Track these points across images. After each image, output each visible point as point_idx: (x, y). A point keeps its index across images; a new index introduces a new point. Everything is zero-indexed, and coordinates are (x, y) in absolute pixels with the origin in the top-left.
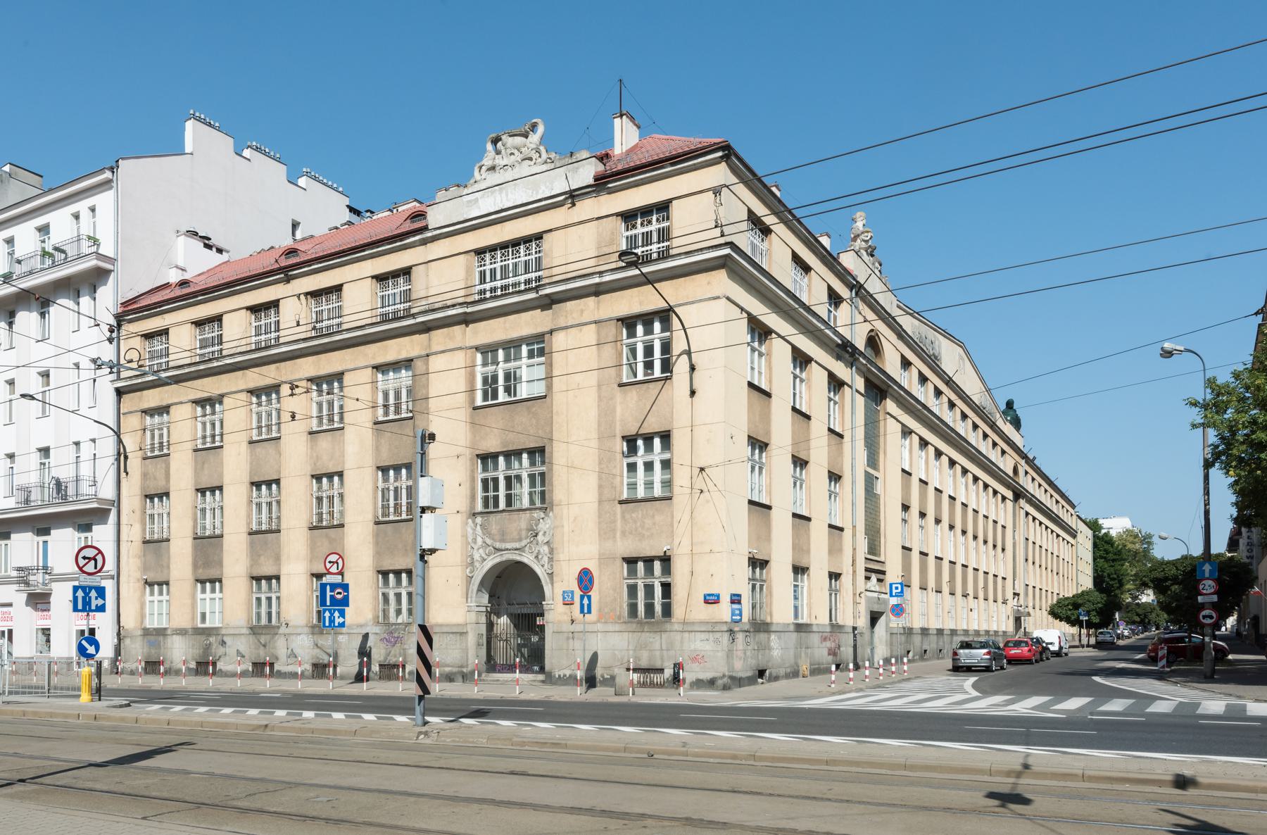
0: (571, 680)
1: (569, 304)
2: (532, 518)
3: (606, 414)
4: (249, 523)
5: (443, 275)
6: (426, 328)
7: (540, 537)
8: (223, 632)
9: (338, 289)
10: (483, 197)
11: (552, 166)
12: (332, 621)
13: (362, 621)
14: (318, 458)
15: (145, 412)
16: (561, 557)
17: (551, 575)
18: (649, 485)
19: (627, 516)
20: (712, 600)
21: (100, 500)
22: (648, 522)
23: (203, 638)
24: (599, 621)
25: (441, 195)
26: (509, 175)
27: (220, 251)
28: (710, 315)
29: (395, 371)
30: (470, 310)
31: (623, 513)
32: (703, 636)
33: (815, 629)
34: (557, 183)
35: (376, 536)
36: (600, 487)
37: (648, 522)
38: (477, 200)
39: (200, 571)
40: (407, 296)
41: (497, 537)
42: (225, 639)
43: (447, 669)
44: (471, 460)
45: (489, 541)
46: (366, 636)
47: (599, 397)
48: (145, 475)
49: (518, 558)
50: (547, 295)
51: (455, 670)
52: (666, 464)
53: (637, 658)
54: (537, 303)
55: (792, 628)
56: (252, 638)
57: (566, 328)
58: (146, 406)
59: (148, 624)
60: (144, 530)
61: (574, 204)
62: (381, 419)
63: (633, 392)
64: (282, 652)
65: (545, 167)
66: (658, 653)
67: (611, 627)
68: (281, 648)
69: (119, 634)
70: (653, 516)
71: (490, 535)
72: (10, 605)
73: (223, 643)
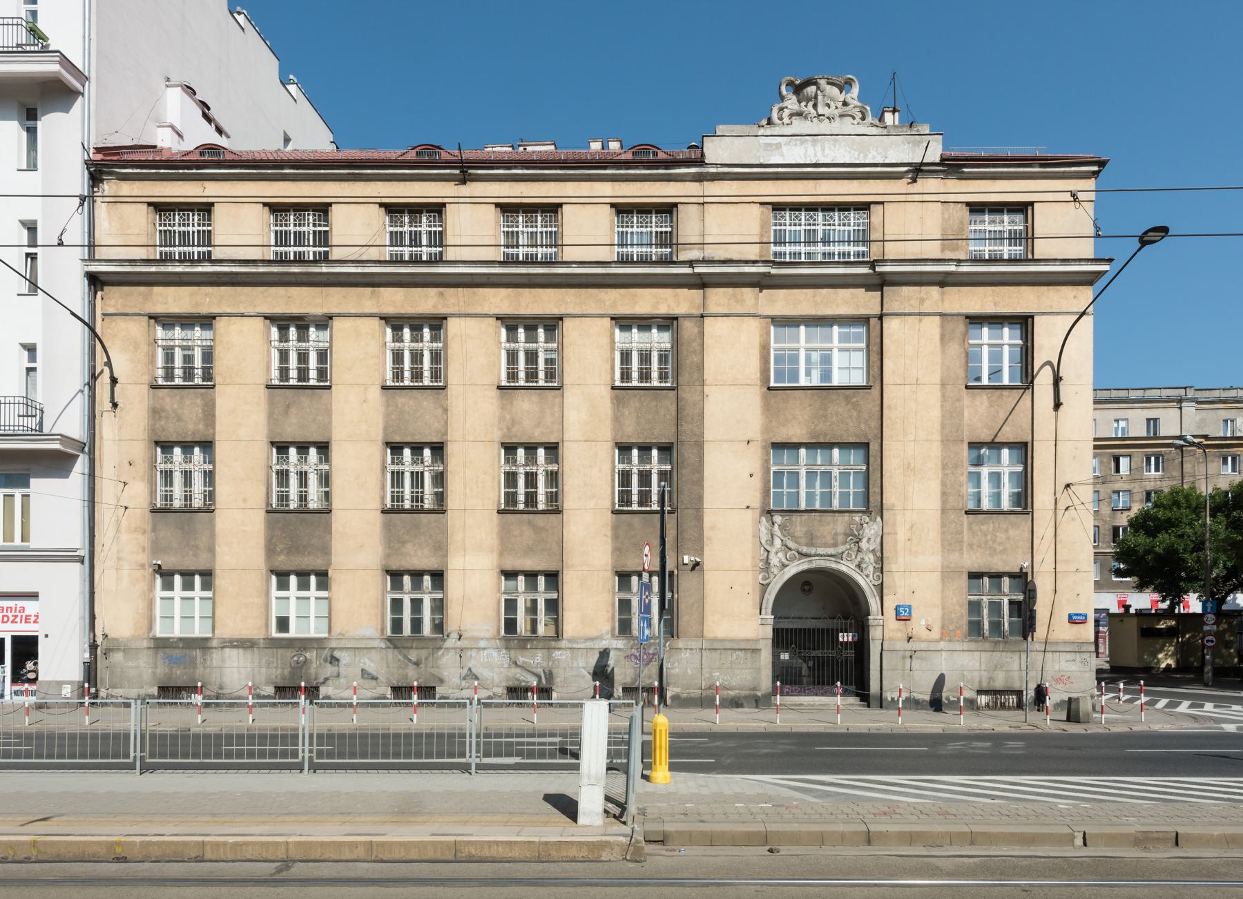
0: (912, 703)
1: (905, 289)
2: (852, 522)
3: (951, 416)
4: (383, 503)
5: (725, 225)
6: (702, 283)
7: (864, 544)
8: (333, 644)
10: (788, 143)
11: (885, 132)
13: (593, 633)
14: (514, 422)
15: (154, 318)
16: (894, 567)
17: (881, 589)
18: (810, 497)
19: (975, 528)
20: (1072, 620)
21: (64, 439)
22: (1001, 536)
23: (289, 653)
24: (941, 639)
25: (721, 129)
26: (825, 127)
28: (1068, 334)
29: (183, 327)
30: (774, 271)
31: (970, 524)
32: (1069, 656)
34: (902, 151)
35: (615, 528)
36: (944, 494)
37: (1001, 536)
38: (779, 146)
39: (282, 558)
40: (666, 240)
41: (803, 541)
42: (337, 654)
43: (732, 693)
44: (764, 448)
45: (791, 544)
46: (604, 654)
47: (943, 396)
48: (156, 413)
49: (834, 566)
50: (699, 274)
51: (744, 693)
52: (325, 479)
53: (991, 679)
54: (861, 281)
56: (391, 654)
57: (905, 315)
58: (159, 309)
59: (159, 632)
60: (153, 493)
61: (914, 181)
62: (275, 382)
63: (983, 399)
66: (1016, 674)
67: (958, 646)
68: (448, 667)
69: (93, 647)
70: (1007, 530)
71: (793, 538)
72: (34, 596)
73: (334, 660)
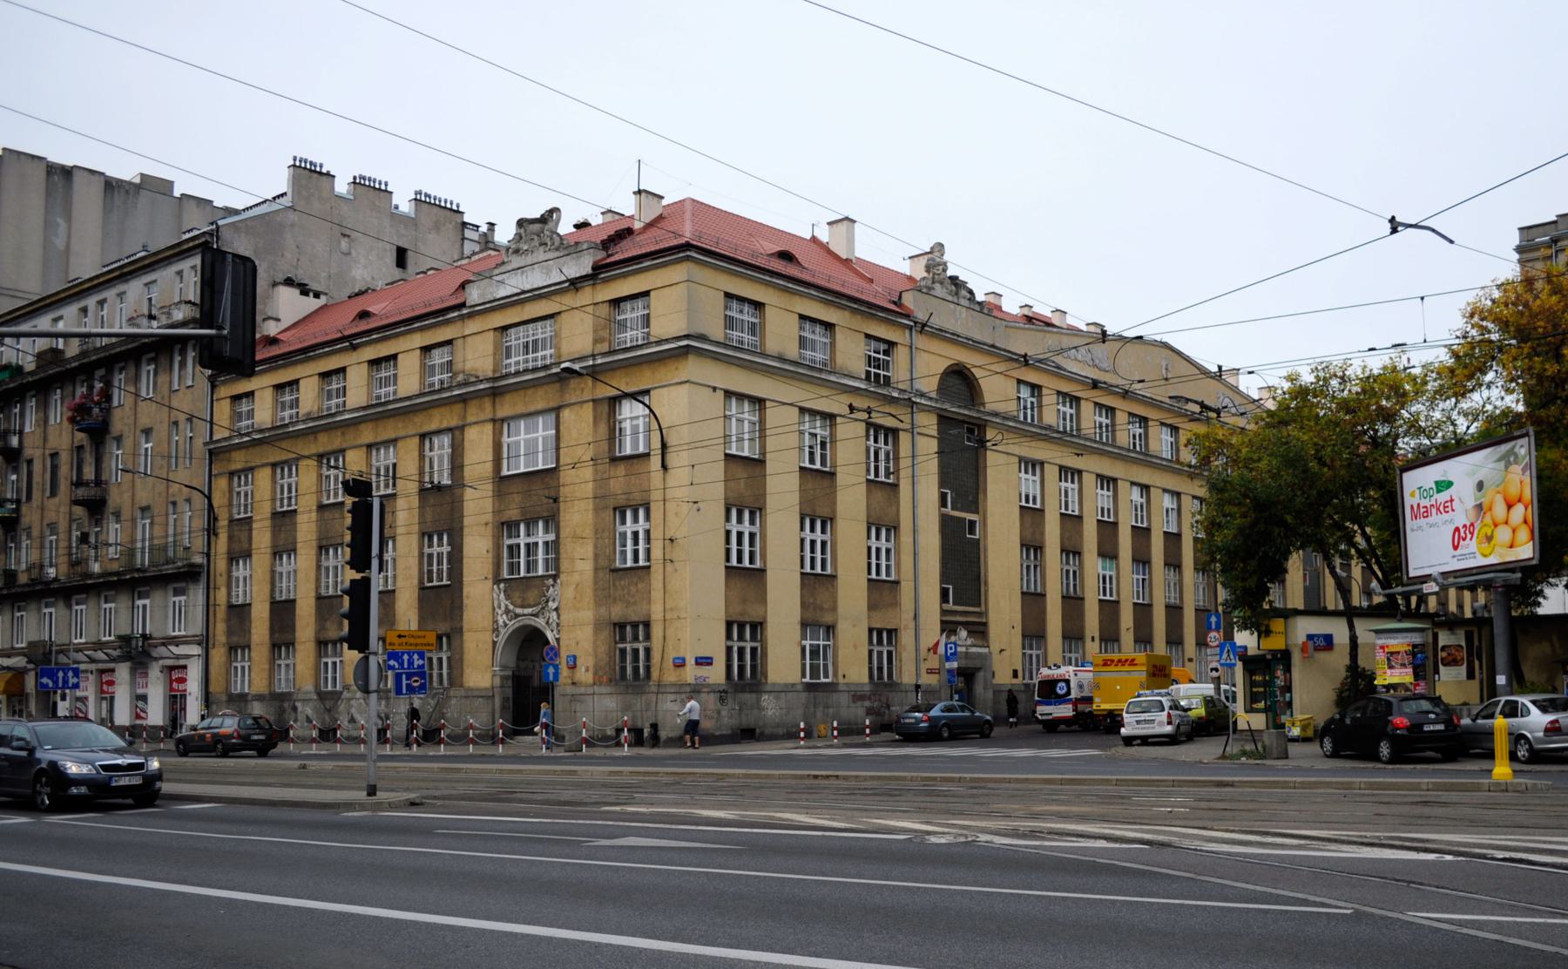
9: (394, 357)
12: (65, 681)
22: (633, 589)
26: (529, 259)
27: (317, 295)
32: (672, 697)
33: (841, 688)
37: (633, 589)
55: (800, 687)
64: (343, 721)
65: (557, 254)
